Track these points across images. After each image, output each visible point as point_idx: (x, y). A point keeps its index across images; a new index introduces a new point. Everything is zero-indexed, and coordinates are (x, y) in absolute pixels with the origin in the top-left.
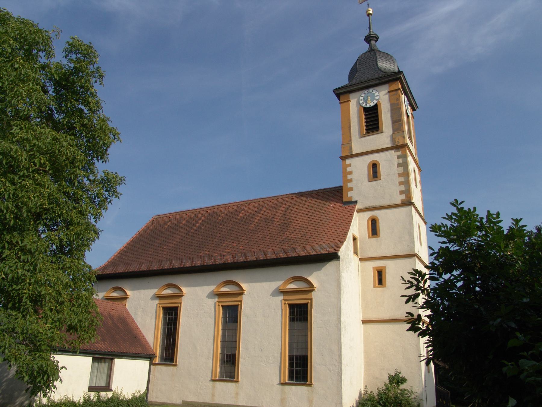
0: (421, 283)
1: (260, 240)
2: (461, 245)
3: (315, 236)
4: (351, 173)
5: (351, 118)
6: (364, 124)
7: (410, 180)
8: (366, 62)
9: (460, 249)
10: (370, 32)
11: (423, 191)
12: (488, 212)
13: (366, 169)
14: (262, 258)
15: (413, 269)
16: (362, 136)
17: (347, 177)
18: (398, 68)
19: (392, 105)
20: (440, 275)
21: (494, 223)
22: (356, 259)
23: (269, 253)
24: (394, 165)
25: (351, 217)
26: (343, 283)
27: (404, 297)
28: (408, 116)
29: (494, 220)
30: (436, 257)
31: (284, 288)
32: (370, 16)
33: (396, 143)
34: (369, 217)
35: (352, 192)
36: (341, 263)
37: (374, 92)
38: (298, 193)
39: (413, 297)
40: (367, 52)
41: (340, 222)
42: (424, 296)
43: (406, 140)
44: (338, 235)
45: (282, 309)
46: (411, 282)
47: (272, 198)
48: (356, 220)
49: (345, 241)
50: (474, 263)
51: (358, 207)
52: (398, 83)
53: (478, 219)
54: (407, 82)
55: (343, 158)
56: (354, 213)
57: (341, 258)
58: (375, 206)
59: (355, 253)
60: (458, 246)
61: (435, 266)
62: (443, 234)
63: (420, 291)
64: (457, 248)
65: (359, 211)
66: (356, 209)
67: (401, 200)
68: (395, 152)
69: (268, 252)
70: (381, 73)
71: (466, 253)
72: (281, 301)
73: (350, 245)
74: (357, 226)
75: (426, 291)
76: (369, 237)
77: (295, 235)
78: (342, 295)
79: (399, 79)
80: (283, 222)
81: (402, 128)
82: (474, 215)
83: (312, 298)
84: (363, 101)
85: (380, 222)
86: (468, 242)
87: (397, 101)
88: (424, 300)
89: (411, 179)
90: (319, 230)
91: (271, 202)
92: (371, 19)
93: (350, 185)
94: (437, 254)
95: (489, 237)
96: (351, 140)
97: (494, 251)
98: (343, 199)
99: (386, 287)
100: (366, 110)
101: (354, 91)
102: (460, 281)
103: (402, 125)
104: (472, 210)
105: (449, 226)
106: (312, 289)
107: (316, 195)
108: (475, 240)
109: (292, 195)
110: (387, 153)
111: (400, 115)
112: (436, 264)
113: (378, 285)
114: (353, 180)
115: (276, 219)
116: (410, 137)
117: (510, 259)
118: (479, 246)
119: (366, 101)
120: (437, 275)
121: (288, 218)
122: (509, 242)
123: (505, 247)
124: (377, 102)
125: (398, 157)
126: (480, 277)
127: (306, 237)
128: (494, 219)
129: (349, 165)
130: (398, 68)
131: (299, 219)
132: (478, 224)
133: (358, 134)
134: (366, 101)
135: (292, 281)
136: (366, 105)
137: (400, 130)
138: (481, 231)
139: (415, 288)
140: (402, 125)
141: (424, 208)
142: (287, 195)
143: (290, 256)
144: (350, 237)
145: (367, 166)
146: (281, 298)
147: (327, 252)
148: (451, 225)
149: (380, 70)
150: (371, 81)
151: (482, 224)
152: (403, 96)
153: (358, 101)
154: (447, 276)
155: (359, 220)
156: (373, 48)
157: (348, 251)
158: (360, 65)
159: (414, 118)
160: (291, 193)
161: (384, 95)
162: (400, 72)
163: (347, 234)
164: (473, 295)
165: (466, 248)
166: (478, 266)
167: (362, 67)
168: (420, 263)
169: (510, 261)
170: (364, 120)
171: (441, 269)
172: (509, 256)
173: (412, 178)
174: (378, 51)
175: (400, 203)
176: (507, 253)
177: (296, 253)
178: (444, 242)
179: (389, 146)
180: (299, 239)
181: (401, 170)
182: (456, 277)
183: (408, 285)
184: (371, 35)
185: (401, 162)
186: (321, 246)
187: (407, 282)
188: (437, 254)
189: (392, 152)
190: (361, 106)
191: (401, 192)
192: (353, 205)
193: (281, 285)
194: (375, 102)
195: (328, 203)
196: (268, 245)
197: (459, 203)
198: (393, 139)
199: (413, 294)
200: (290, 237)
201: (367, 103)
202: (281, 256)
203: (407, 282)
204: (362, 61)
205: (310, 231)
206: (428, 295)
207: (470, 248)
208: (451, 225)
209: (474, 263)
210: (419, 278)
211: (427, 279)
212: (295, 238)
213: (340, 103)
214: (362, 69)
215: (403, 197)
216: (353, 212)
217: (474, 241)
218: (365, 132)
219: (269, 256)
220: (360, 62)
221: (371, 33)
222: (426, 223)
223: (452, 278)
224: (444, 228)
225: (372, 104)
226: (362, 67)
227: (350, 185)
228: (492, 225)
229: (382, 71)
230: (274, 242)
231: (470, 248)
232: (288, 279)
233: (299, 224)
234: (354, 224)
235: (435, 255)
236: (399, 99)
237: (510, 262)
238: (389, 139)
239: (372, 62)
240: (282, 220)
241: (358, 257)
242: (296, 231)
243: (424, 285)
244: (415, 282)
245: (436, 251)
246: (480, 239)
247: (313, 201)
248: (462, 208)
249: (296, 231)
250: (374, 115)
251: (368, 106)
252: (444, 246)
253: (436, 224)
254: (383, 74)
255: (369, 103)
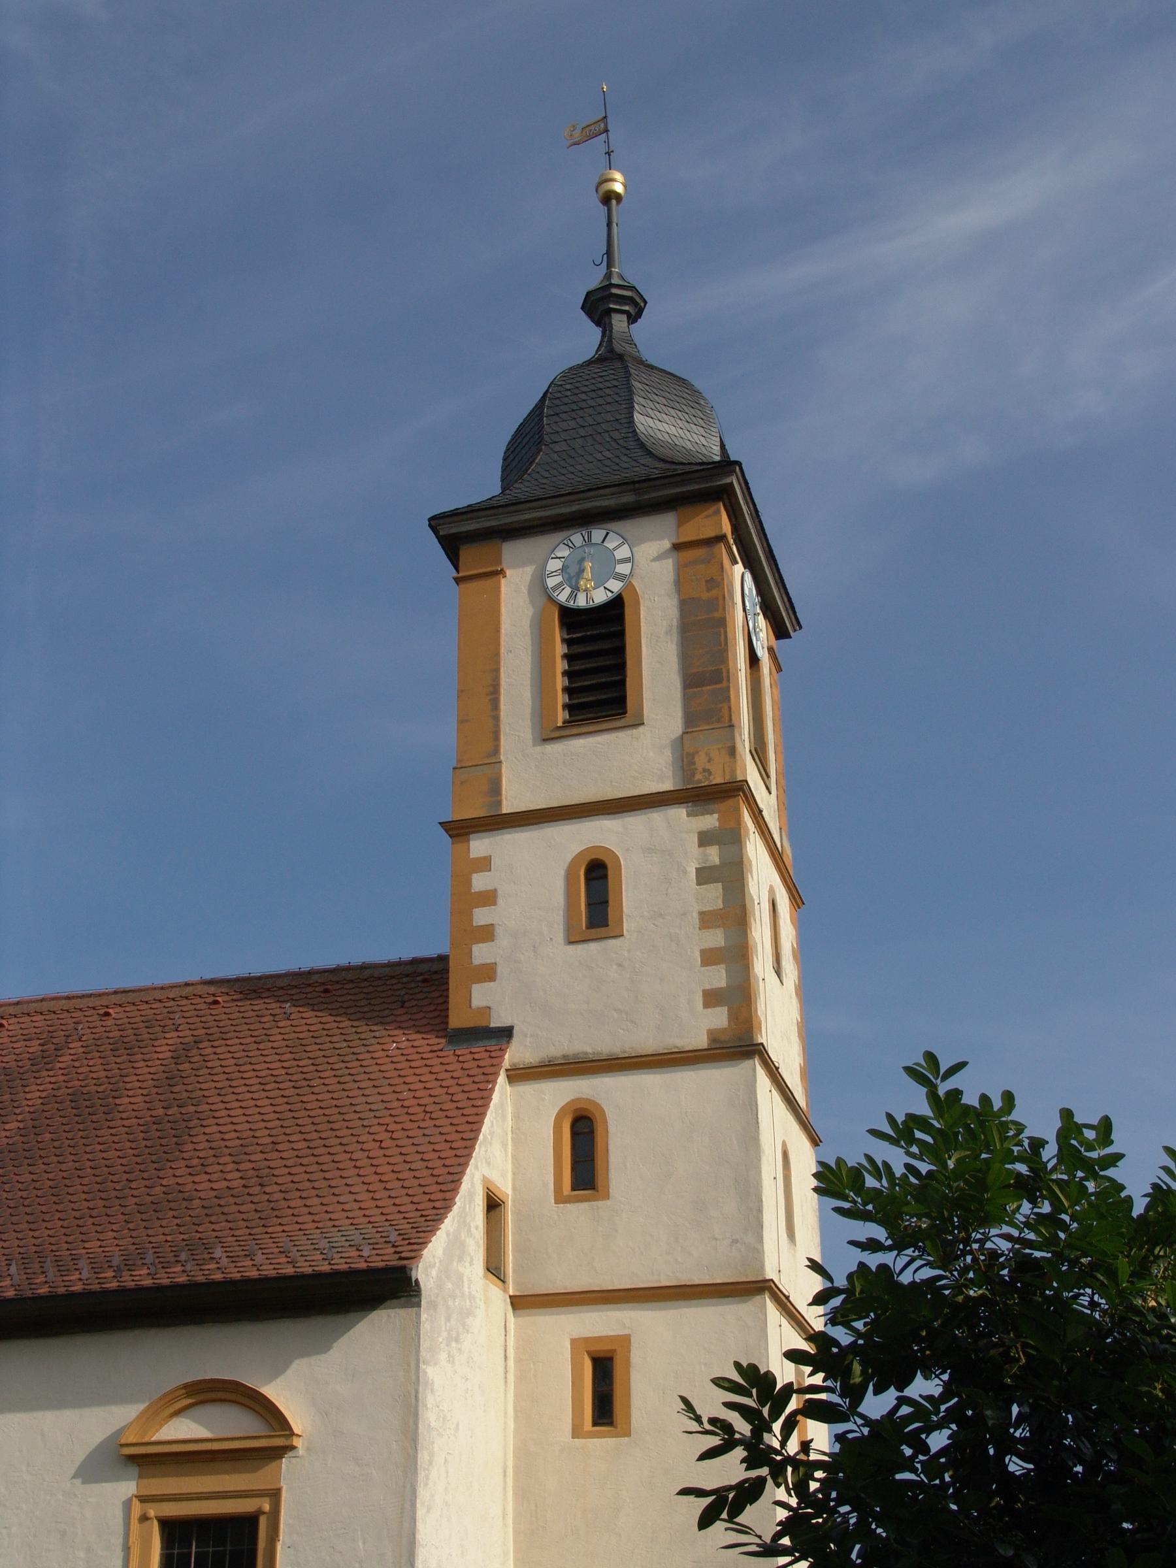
0: (770, 1430)
1: (42, 1201)
2: (945, 1262)
3: (308, 1184)
4: (489, 898)
5: (502, 650)
6: (560, 682)
7: (751, 943)
8: (583, 405)
9: (940, 1278)
10: (609, 275)
11: (806, 993)
12: (1067, 1114)
13: (559, 884)
14: (44, 1291)
15: (737, 1365)
16: (549, 735)
17: (471, 915)
18: (723, 446)
19: (686, 605)
20: (855, 1395)
21: (1092, 1169)
22: (496, 1299)
23: (83, 1263)
24: (685, 872)
25: (479, 1103)
26: (430, 1416)
27: (692, 1498)
28: (754, 660)
29: (1085, 1154)
30: (835, 1310)
31: (146, 1439)
32: (614, 202)
33: (698, 777)
34: (563, 1104)
35: (492, 984)
36: (424, 1316)
37: (610, 545)
38: (237, 980)
39: (731, 1496)
40: (589, 363)
41: (429, 1123)
42: (781, 1494)
43: (739, 762)
44: (417, 1182)
45: (127, 1549)
46: (726, 1428)
47: (114, 999)
48: (504, 1117)
49: (450, 1215)
50: (1001, 1343)
51: (514, 1054)
52: (718, 512)
53: (1020, 1144)
54: (757, 511)
55: (459, 830)
56: (494, 1082)
57: (424, 1293)
58: (591, 1057)
59: (495, 1268)
60: (929, 1264)
61: (835, 1350)
62: (870, 1207)
63: (764, 1471)
64: (927, 1273)
65: (518, 1075)
66: (506, 1064)
67: (710, 1033)
68: (688, 815)
69: (75, 1259)
70: (648, 461)
71: (968, 1297)
72: (127, 1505)
73: (469, 1231)
74: (504, 1145)
75: (790, 1469)
76: (560, 1199)
77: (215, 1177)
78: (421, 1474)
79: (724, 495)
80: (161, 1112)
81: (725, 710)
82: (1004, 1126)
83: (279, 1490)
84: (559, 579)
85: (612, 1128)
86: (975, 1246)
87: (708, 590)
88: (782, 1514)
89: (758, 940)
90: (328, 1158)
91: (107, 1014)
92: (615, 219)
93: (481, 953)
94: (843, 1296)
95: (1065, 1227)
96: (496, 750)
97: (1089, 1291)
98: (447, 1016)
99: (627, 1433)
100: (571, 618)
101: (524, 528)
102: (939, 1426)
103: (728, 699)
104: (997, 1104)
105: (899, 1171)
106: (279, 1442)
107: (326, 991)
108: (1007, 1237)
109: (212, 989)
110: (658, 817)
111: (722, 652)
112: (836, 1343)
113: (595, 1424)
114: (499, 931)
115: (127, 1100)
116: (759, 754)
117: (1155, 1332)
118: (1024, 1265)
119: (573, 577)
120: (841, 1396)
121: (185, 1095)
122: (1151, 1251)
123: (1134, 1274)
124: (625, 588)
125: (705, 839)
126: (1026, 1409)
127: (268, 1189)
128: (1090, 1147)
129: (484, 864)
130: (723, 446)
131: (237, 1104)
132: (1022, 1168)
133: (529, 723)
134: (573, 577)
135: (189, 1401)
136: (573, 596)
137: (719, 721)
138: (1034, 1202)
139: (745, 1454)
140: (725, 696)
141: (808, 1073)
142: (187, 984)
143: (183, 1279)
144: (471, 1194)
145: (562, 873)
146: (128, 1488)
147: (362, 1265)
148: (908, 1166)
149: (642, 445)
150: (601, 492)
151: (1038, 1168)
152: (739, 568)
153: (541, 577)
154: (876, 1405)
155: (517, 1117)
156: (618, 347)
157: (460, 1259)
158: (556, 418)
159: (779, 669)
160: (208, 976)
161: (652, 561)
162: (728, 465)
163: (457, 1182)
164: (997, 1493)
165: (971, 1275)
166: (1019, 1360)
167: (564, 425)
168: (784, 1322)
169: (1157, 1341)
170: (561, 665)
171: (857, 1368)
172: (1151, 1318)
173: (760, 933)
174: (641, 362)
175: (705, 1046)
176: (1145, 1300)
177: (213, 1266)
178: (872, 1245)
179: (667, 785)
180: (232, 1200)
181: (713, 896)
182: (920, 1412)
183: (715, 1441)
184: (614, 291)
185: (717, 861)
186: (337, 1237)
187: (708, 1427)
188: (843, 1296)
189: (679, 813)
190: (552, 600)
191: (712, 998)
192: (492, 1044)
193: (131, 1423)
194: (615, 586)
195: (380, 1031)
196: (81, 1222)
197: (942, 1072)
198: (685, 759)
199: (733, 1483)
200: (190, 1187)
201: (576, 589)
202: (142, 1277)
203: (708, 1427)
204: (566, 400)
205: (289, 1163)
206: (800, 1489)
207: (985, 1273)
208: (908, 1166)
209: (1001, 1343)
210: (763, 1406)
211: (794, 1413)
212: (214, 1193)
213: (458, 581)
214: (564, 435)
215: (719, 1018)
216: (491, 1078)
217: (1005, 1245)
218: (561, 716)
219: (79, 1280)
220: (557, 402)
221: (615, 281)
222: (815, 1141)
223: (905, 1410)
224: (879, 1179)
225: (600, 597)
226: (564, 425)
227: (481, 953)
228: (1080, 1174)
229: (649, 453)
230: (109, 1211)
231: (985, 1273)
232: (165, 1395)
233: (238, 1127)
234: (492, 1134)
235: (836, 1302)
236: (717, 583)
237: (1154, 1344)
238: (668, 753)
239: (608, 408)
240: (158, 1104)
241: (505, 1290)
242: (221, 1160)
243: (783, 1443)
244: (743, 1427)
245: (841, 1282)
246: (1032, 1236)
247: (307, 1021)
248: (956, 1094)
249: (221, 1160)
250: (605, 645)
251: (581, 602)
252: (873, 1260)
253: (839, 1161)
254: (654, 469)
255: (586, 590)
